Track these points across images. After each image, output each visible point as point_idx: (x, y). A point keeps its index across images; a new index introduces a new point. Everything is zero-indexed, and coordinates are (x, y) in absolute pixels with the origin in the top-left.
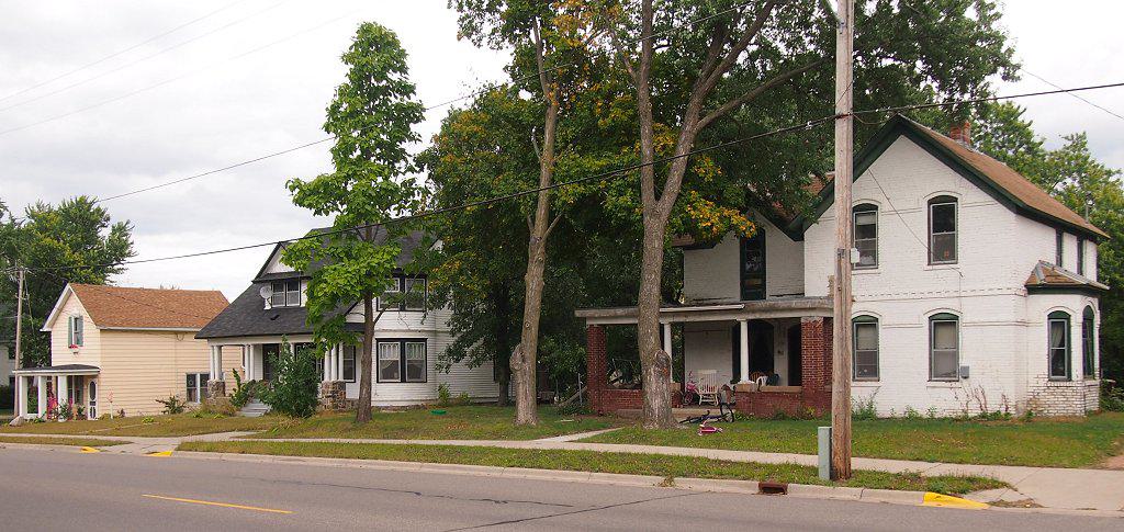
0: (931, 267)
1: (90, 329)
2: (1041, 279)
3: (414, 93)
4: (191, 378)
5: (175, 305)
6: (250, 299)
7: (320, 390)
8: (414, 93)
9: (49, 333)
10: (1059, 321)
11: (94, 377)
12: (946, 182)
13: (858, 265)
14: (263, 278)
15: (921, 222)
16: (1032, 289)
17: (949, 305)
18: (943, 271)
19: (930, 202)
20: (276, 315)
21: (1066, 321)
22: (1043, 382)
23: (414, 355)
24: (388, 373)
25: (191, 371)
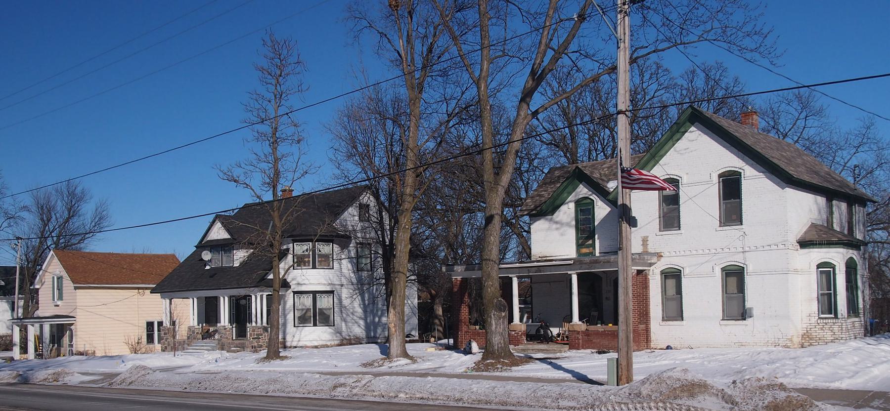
0: (721, 228)
1: (68, 284)
2: (814, 236)
3: (7, 188)
4: (150, 325)
5: (137, 266)
6: (195, 258)
7: (248, 330)
8: (7, 188)
9: (38, 289)
10: (826, 271)
11: (72, 324)
12: (731, 161)
13: (835, 315)
14: (203, 245)
15: (713, 191)
16: (804, 244)
17: (737, 259)
18: (732, 231)
19: (720, 176)
20: (215, 272)
21: (831, 269)
22: (814, 319)
23: (324, 303)
24: (303, 320)
25: (150, 320)
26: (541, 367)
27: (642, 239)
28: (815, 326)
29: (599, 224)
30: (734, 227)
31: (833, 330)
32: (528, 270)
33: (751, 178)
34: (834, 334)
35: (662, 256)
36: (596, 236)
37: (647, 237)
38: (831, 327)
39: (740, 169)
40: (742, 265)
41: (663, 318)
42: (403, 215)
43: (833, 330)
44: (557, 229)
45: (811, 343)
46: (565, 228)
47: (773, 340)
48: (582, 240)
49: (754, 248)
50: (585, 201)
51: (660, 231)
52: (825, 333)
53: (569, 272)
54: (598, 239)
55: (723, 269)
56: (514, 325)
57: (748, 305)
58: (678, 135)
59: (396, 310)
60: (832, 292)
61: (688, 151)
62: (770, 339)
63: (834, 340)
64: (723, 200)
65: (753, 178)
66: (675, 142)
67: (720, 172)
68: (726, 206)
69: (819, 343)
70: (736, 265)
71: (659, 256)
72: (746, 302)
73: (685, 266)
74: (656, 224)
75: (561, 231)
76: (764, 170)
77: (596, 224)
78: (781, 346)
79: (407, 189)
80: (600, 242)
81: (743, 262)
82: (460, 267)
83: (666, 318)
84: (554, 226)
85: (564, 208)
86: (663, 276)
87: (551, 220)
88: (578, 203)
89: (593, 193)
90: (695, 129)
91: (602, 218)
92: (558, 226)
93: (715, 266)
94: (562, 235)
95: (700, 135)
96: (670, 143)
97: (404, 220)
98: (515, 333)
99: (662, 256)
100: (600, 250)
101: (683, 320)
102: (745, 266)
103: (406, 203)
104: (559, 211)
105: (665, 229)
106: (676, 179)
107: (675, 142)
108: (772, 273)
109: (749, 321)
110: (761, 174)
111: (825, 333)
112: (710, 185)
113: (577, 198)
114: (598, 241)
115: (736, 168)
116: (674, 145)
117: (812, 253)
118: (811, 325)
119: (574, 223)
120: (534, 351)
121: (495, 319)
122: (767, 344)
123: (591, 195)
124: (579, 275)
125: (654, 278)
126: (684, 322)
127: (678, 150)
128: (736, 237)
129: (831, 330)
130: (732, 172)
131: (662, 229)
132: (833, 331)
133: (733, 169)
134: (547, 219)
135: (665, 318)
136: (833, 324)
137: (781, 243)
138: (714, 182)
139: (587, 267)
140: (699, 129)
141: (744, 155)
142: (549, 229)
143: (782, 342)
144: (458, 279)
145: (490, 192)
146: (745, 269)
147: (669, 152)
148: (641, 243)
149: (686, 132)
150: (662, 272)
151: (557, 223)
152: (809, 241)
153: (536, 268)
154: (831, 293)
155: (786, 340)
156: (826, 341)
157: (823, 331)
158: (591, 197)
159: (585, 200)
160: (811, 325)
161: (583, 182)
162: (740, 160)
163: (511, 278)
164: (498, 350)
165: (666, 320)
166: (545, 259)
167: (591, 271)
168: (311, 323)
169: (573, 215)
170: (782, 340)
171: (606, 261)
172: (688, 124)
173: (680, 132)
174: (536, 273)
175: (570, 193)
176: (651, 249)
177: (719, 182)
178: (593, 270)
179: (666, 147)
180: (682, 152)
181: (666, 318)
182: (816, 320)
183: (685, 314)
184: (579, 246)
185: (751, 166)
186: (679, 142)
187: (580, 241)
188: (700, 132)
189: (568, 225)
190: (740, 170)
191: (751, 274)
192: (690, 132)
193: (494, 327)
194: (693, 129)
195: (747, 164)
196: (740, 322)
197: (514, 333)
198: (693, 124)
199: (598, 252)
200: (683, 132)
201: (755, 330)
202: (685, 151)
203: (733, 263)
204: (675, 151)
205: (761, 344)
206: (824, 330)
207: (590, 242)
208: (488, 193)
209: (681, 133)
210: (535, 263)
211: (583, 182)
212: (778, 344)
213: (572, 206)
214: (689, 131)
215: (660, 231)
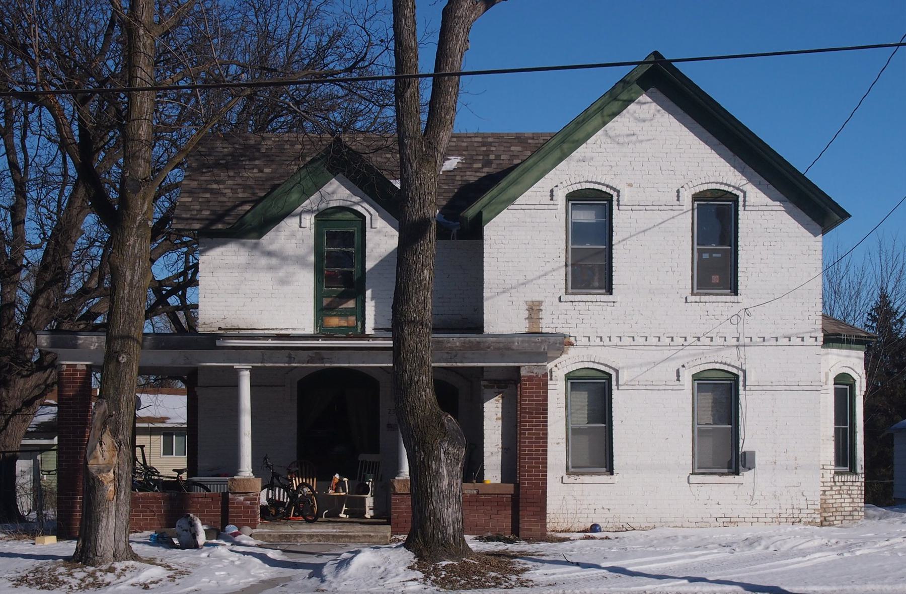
17: (727, 359)
19: (696, 197)
26: (728, 576)
27: (527, 307)
28: (831, 487)
29: (376, 266)
30: (720, 298)
31: (852, 494)
32: (290, 357)
33: (757, 208)
34: (853, 502)
35: (571, 344)
36: (369, 293)
37: (540, 303)
38: (849, 490)
39: (738, 189)
40: (735, 371)
41: (567, 468)
42: (141, 193)
43: (852, 494)
44: (271, 268)
45: (825, 518)
46: (292, 269)
47: (790, 511)
48: (330, 299)
49: (759, 340)
50: (339, 216)
51: (567, 293)
52: (842, 500)
53: (237, 366)
54: (372, 299)
55: (696, 377)
56: (243, 480)
57: (746, 445)
58: (615, 106)
59: (121, 437)
60: (848, 426)
61: (634, 138)
62: (784, 511)
63: (853, 511)
64: (698, 244)
65: (759, 208)
66: (607, 119)
67: (697, 190)
68: (700, 256)
69: (835, 516)
70: (588, 368)
71: (562, 343)
72: (741, 441)
73: (621, 365)
74: (559, 278)
75: (281, 273)
76: (782, 196)
77: (369, 265)
78: (805, 522)
79: (140, 126)
80: (376, 307)
81: (737, 364)
82: (95, 338)
83: (574, 469)
84: (263, 261)
85: (290, 224)
86: (569, 385)
87: (255, 247)
88: (323, 217)
89: (364, 200)
90: (649, 99)
91: (386, 254)
92: (274, 261)
93: (681, 370)
94: (283, 282)
95: (659, 111)
96: (597, 120)
97: (142, 205)
98: (246, 500)
99: (571, 344)
100: (376, 323)
101: (612, 474)
102: (741, 374)
103: (142, 162)
104: (278, 231)
105: (575, 291)
106: (605, 192)
107: (607, 119)
108: (792, 388)
109: (746, 476)
110: (778, 203)
111: (842, 500)
112: (676, 213)
113: (323, 206)
114: (373, 303)
115: (729, 186)
116: (604, 124)
117: (830, 356)
118: (825, 484)
119: (312, 258)
120: (315, 539)
121: (447, 464)
122: (778, 519)
123: (358, 204)
124: (253, 371)
125: (680, 387)
126: (615, 478)
127: (611, 133)
128: (726, 318)
129: (850, 495)
130: (720, 194)
131: (570, 291)
132: (852, 496)
133: (723, 187)
134: (244, 245)
135: (571, 470)
136: (851, 484)
137: (809, 335)
138: (685, 208)
139: (445, 356)
140: (655, 100)
141: (745, 164)
142: (248, 267)
143: (805, 516)
144: (78, 368)
145: (420, 165)
146: (741, 379)
147: (593, 137)
148: (526, 314)
149: (631, 101)
150: (568, 377)
151: (270, 254)
152: (833, 335)
153: (310, 353)
154: (847, 428)
155: (813, 511)
156: (844, 513)
157: (840, 496)
158: (359, 208)
159: (340, 212)
160: (825, 484)
161: (340, 175)
162: (737, 173)
163: (236, 374)
164: (454, 537)
165: (577, 474)
166: (236, 332)
167: (454, 364)
168: (847, 466)
169: (311, 242)
170: (807, 511)
171: (501, 345)
172: (636, 87)
173: (619, 100)
174: (308, 363)
175: (306, 195)
176: (546, 326)
177: (693, 209)
178: (459, 365)
179: (588, 127)
180: (621, 140)
181: (574, 469)
182: (832, 476)
183: (618, 461)
184: (322, 311)
185: (758, 186)
186: (616, 119)
187: (326, 301)
188: (659, 108)
189: (300, 261)
190: (735, 192)
191: (752, 388)
192: (639, 103)
193: (446, 482)
194: (644, 98)
195: (750, 180)
196: (730, 479)
197: (242, 498)
198: (645, 88)
199: (373, 326)
200: (624, 101)
201: (757, 493)
202: (626, 140)
203: (717, 366)
204: (606, 134)
205: (765, 520)
206: (841, 494)
207: (351, 304)
208: (415, 166)
209: (620, 103)
210: (270, 341)
211: (340, 175)
212: (798, 520)
213: (309, 220)
214: (636, 101)
215: (693, 294)
